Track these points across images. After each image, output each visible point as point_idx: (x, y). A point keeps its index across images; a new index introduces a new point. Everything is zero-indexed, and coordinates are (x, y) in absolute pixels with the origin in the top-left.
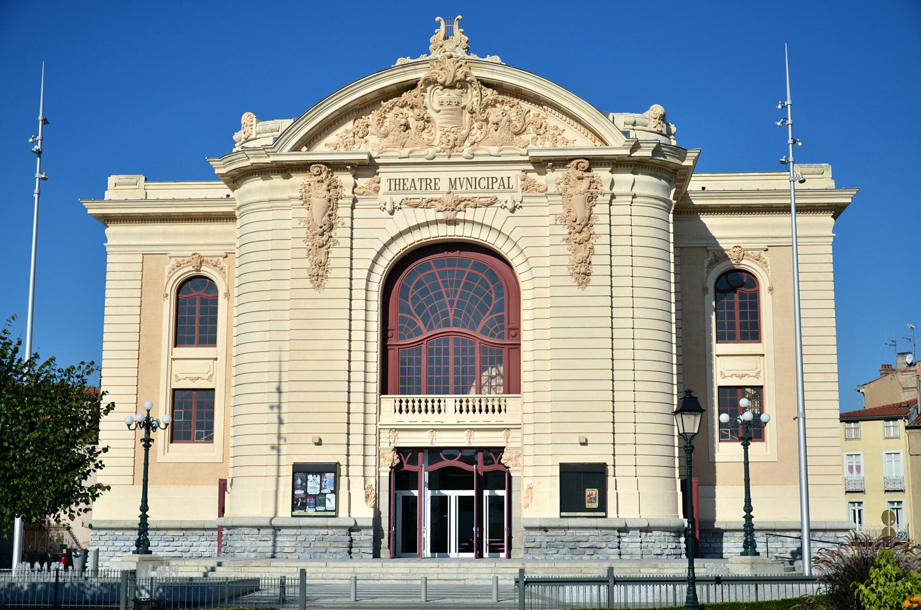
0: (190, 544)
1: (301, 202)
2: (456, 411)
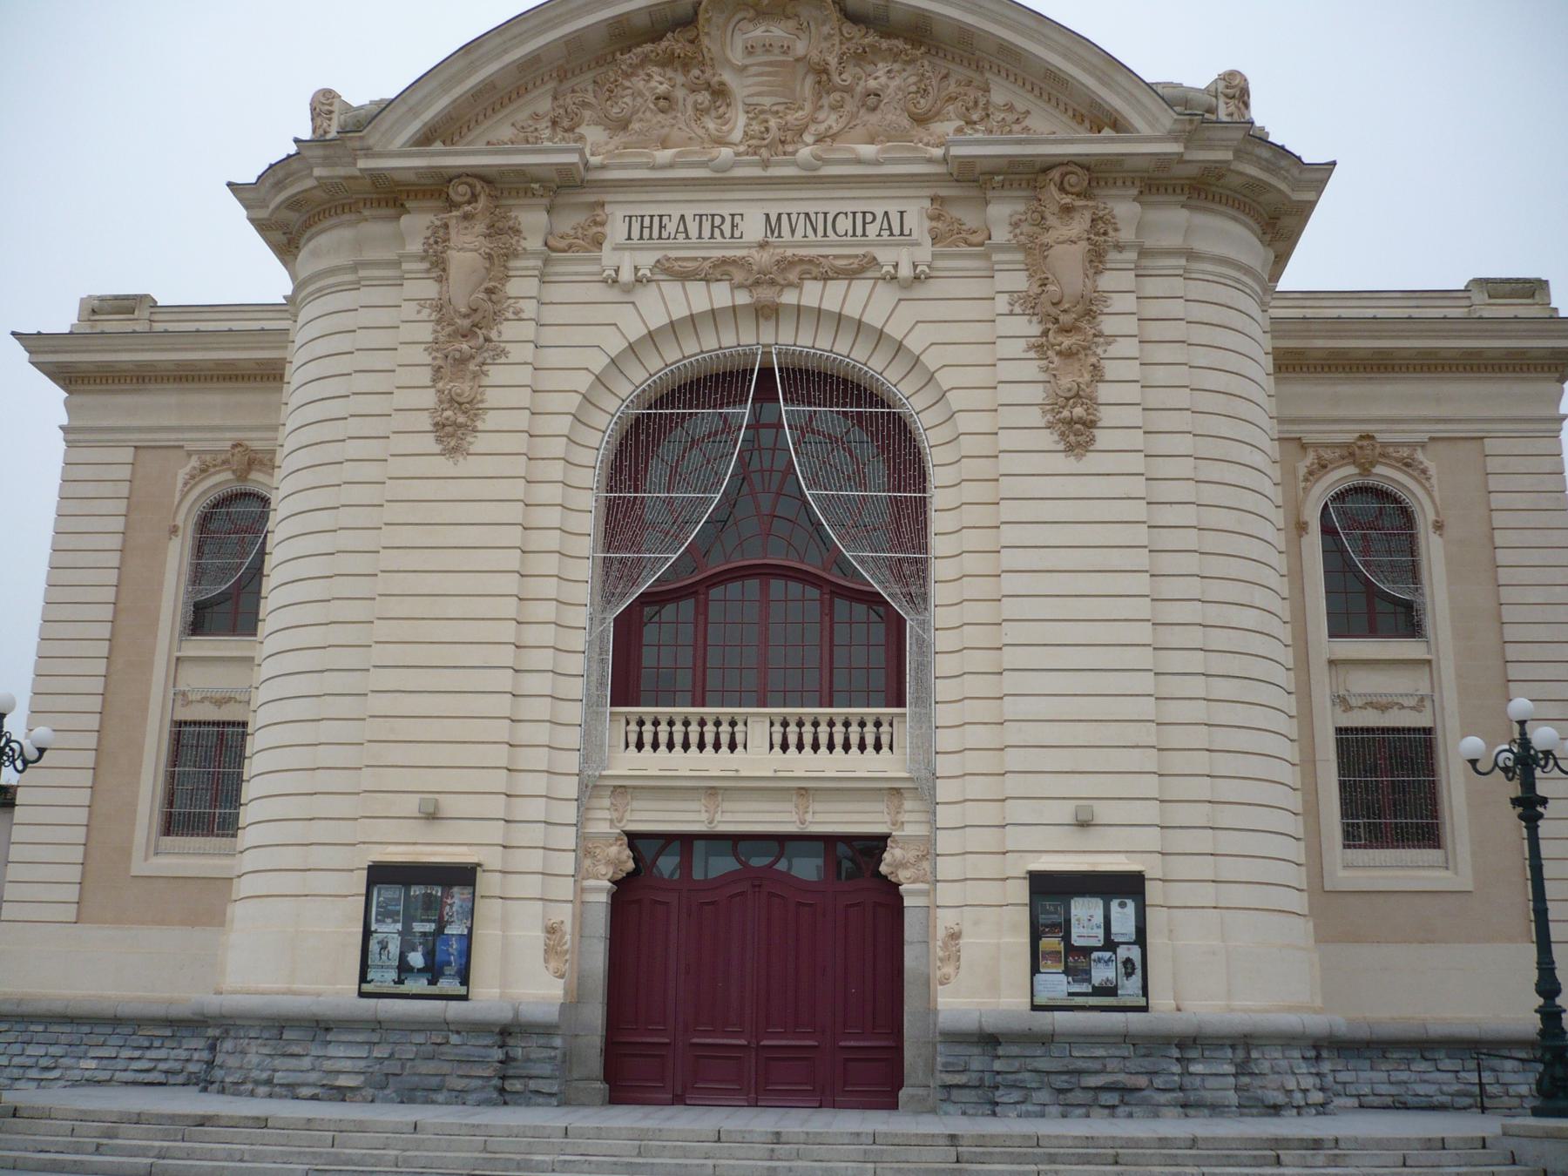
0: (184, 1054)
1: (425, 265)
2: (772, 747)
